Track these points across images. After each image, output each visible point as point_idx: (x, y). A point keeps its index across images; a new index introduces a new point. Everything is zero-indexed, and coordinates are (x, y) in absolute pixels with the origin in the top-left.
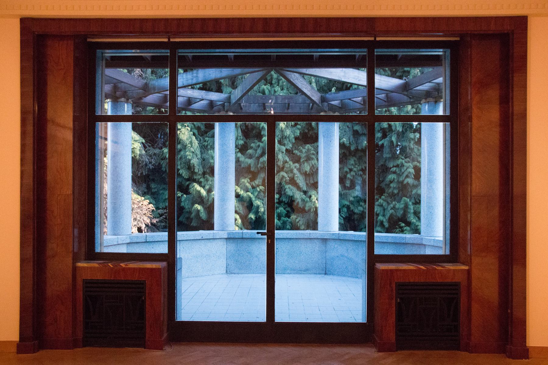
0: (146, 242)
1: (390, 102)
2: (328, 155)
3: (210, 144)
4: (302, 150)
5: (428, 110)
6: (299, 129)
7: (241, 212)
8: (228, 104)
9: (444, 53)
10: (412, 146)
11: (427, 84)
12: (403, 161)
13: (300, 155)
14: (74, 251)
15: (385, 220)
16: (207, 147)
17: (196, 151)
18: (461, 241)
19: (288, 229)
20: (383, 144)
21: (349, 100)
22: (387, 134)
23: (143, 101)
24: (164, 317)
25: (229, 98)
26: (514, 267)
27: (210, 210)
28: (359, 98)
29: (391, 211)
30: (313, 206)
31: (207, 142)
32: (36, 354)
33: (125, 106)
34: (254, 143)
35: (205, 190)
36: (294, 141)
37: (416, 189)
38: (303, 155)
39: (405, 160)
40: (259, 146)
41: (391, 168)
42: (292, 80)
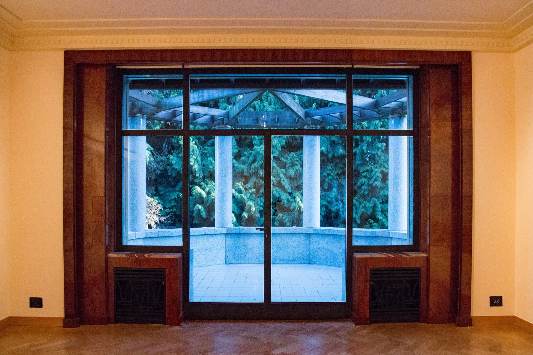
0: (159, 237)
1: (363, 117)
2: (311, 162)
3: (209, 152)
4: (287, 157)
5: (394, 124)
6: (284, 139)
7: (236, 212)
8: (227, 118)
9: (408, 79)
10: (380, 154)
11: (393, 103)
12: (373, 167)
13: (285, 162)
14: (106, 244)
15: (357, 217)
16: (206, 155)
17: (197, 158)
18: (422, 233)
19: (276, 226)
20: (355, 152)
21: (328, 116)
22: (359, 144)
23: (156, 116)
24: (181, 299)
25: (228, 113)
26: (463, 254)
27: (210, 209)
28: (337, 114)
29: (362, 210)
30: (297, 206)
31: (207, 150)
32: (79, 328)
33: (140, 121)
34: (247, 151)
35: (205, 192)
36: (280, 149)
37: (383, 191)
38: (289, 162)
39: (374, 166)
40: (251, 154)
41: (362, 173)
42: (282, 99)
